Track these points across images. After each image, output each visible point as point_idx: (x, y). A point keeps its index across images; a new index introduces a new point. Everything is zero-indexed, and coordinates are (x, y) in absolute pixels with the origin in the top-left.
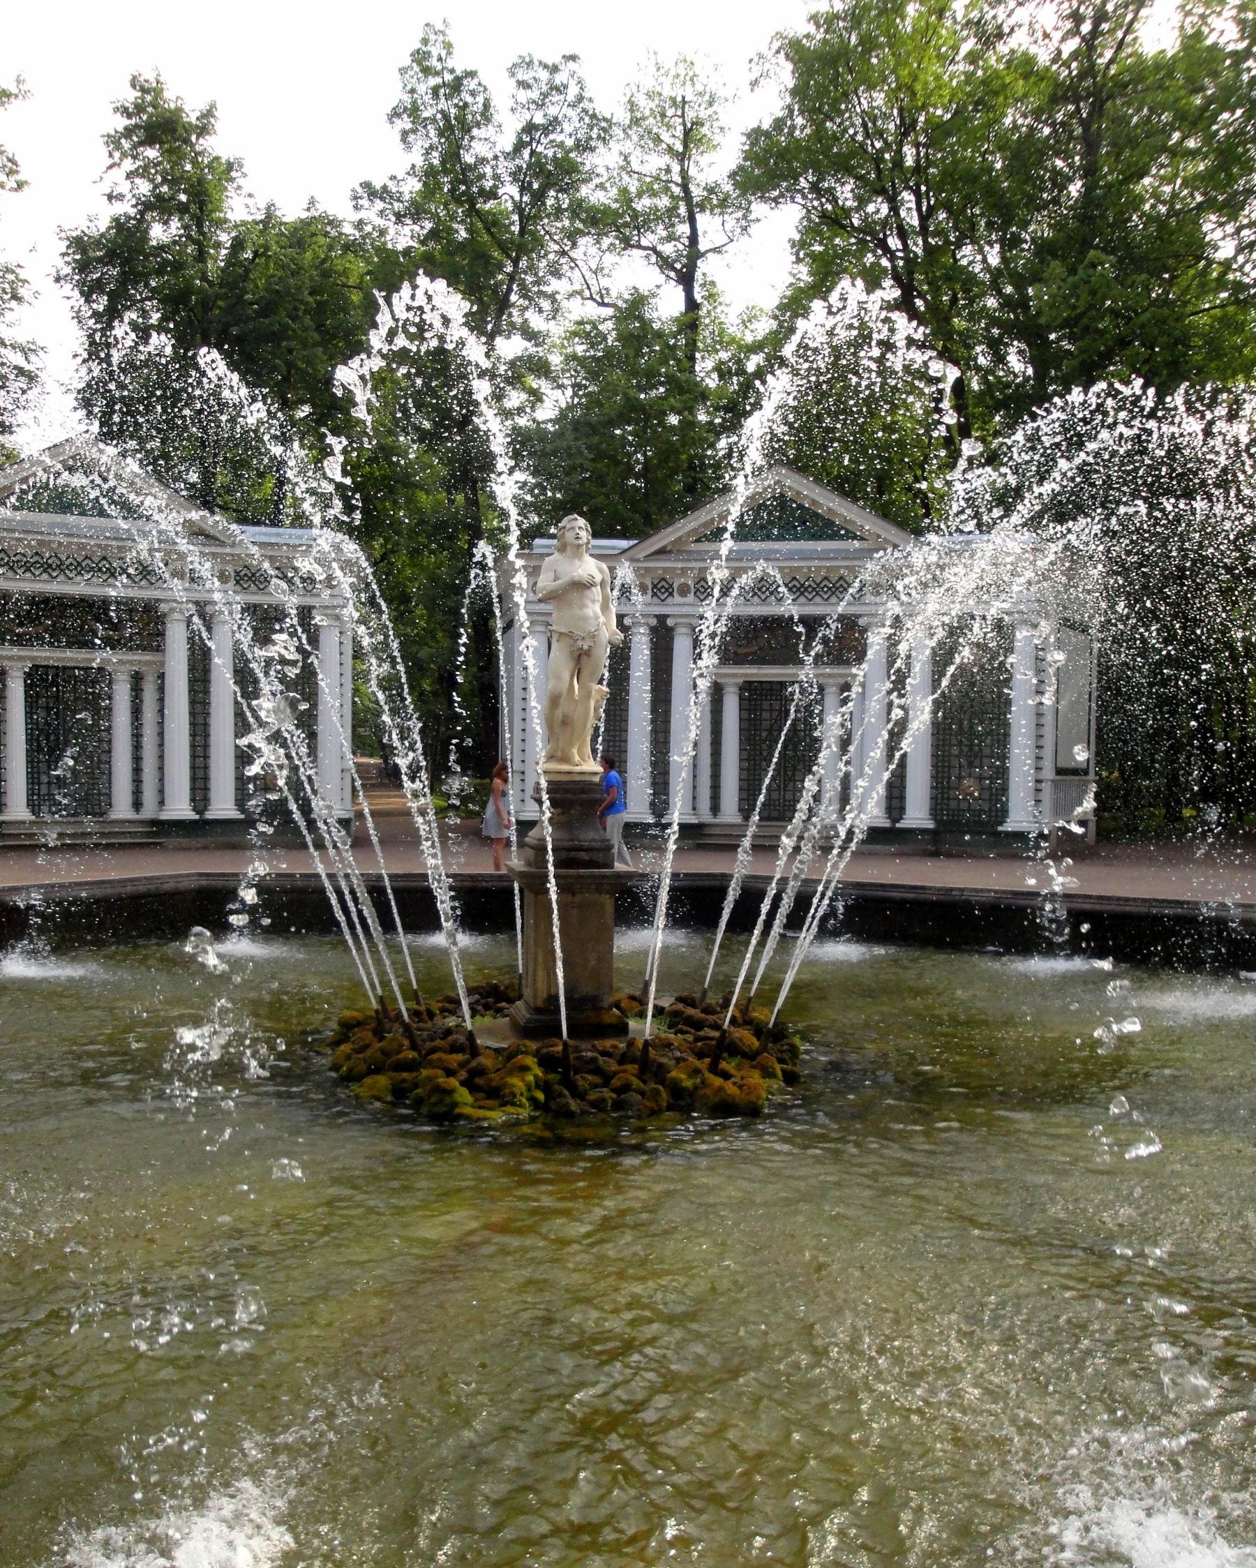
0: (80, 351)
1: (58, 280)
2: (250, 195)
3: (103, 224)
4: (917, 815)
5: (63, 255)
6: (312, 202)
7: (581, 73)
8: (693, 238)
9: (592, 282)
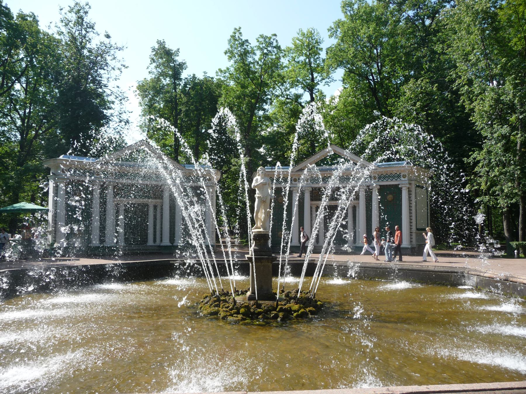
7: (277, 38)
8: (313, 79)
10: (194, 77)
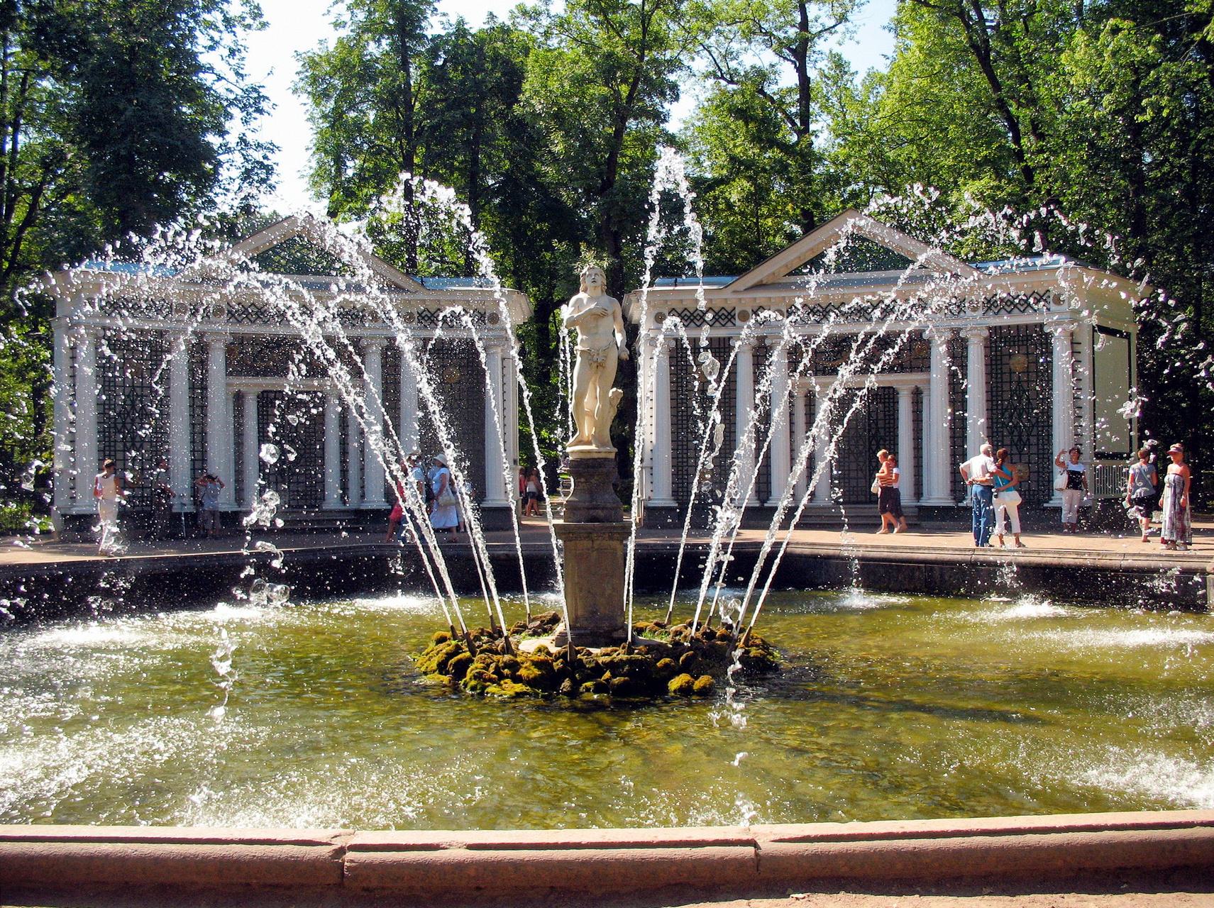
0: (311, 146)
1: (295, 91)
2: (444, 15)
3: (332, 45)
5: (298, 73)
6: (492, 16)
8: (804, 25)
9: (723, 65)
10: (461, 31)
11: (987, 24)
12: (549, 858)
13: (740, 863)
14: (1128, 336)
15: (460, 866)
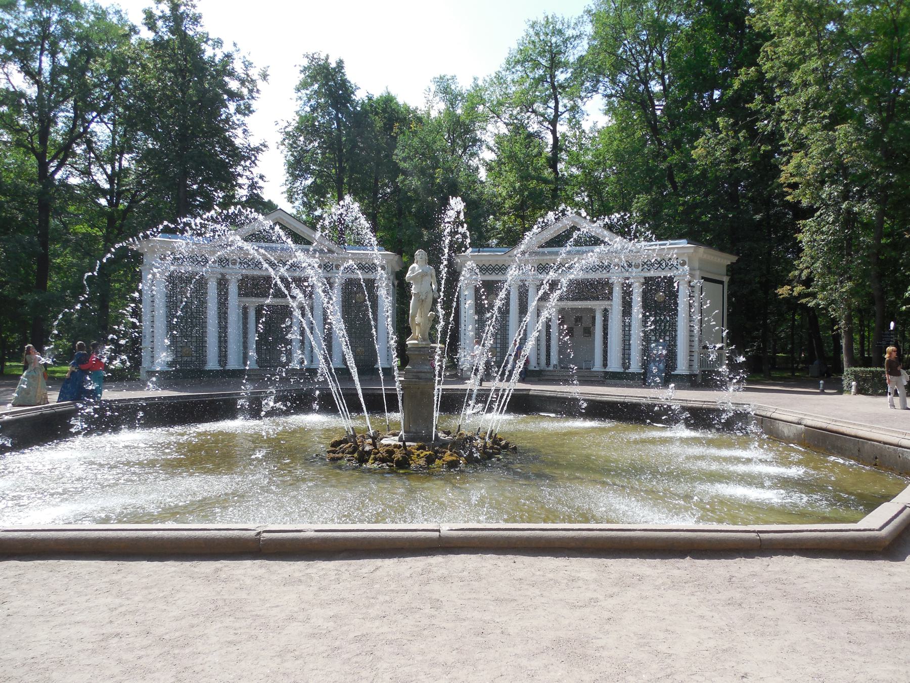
4: (635, 366)
11: (657, 107)
12: (45, 537)
13: (431, 540)
14: (721, 282)
15: (310, 540)
